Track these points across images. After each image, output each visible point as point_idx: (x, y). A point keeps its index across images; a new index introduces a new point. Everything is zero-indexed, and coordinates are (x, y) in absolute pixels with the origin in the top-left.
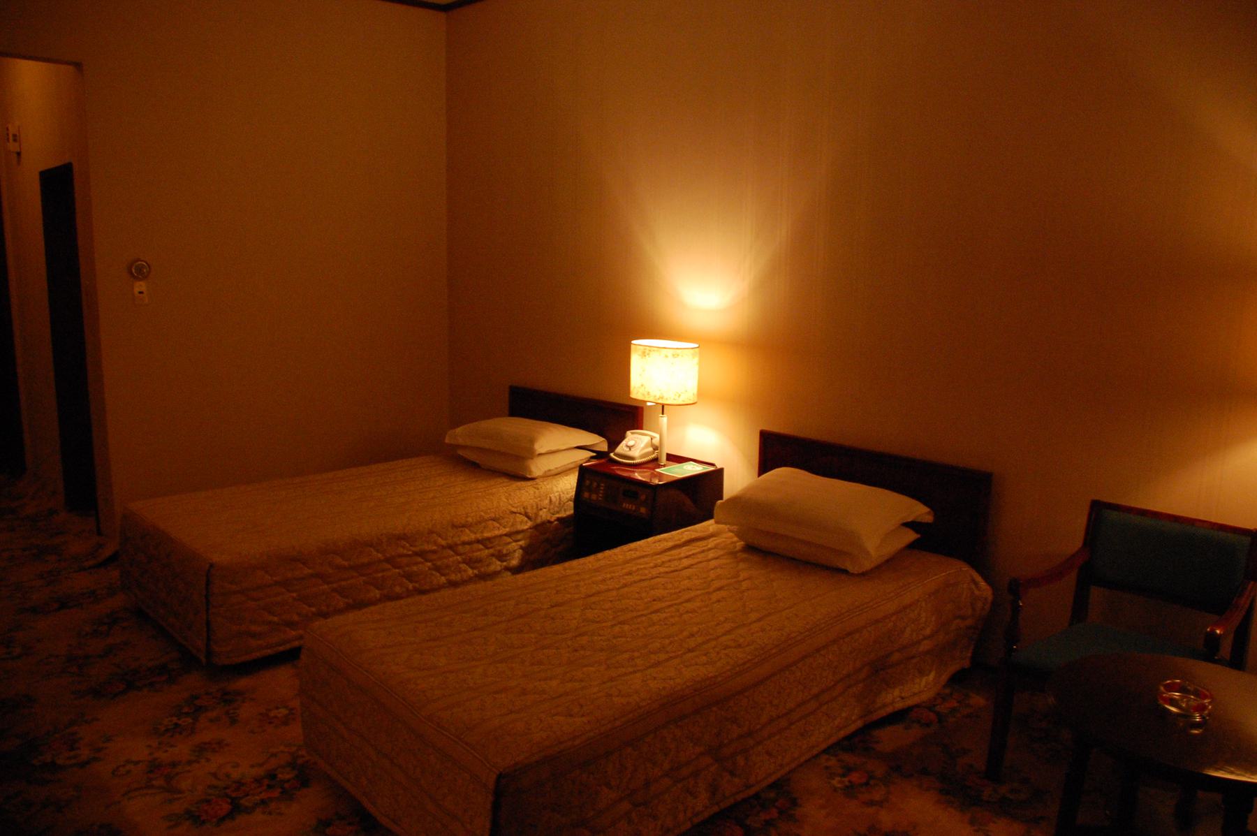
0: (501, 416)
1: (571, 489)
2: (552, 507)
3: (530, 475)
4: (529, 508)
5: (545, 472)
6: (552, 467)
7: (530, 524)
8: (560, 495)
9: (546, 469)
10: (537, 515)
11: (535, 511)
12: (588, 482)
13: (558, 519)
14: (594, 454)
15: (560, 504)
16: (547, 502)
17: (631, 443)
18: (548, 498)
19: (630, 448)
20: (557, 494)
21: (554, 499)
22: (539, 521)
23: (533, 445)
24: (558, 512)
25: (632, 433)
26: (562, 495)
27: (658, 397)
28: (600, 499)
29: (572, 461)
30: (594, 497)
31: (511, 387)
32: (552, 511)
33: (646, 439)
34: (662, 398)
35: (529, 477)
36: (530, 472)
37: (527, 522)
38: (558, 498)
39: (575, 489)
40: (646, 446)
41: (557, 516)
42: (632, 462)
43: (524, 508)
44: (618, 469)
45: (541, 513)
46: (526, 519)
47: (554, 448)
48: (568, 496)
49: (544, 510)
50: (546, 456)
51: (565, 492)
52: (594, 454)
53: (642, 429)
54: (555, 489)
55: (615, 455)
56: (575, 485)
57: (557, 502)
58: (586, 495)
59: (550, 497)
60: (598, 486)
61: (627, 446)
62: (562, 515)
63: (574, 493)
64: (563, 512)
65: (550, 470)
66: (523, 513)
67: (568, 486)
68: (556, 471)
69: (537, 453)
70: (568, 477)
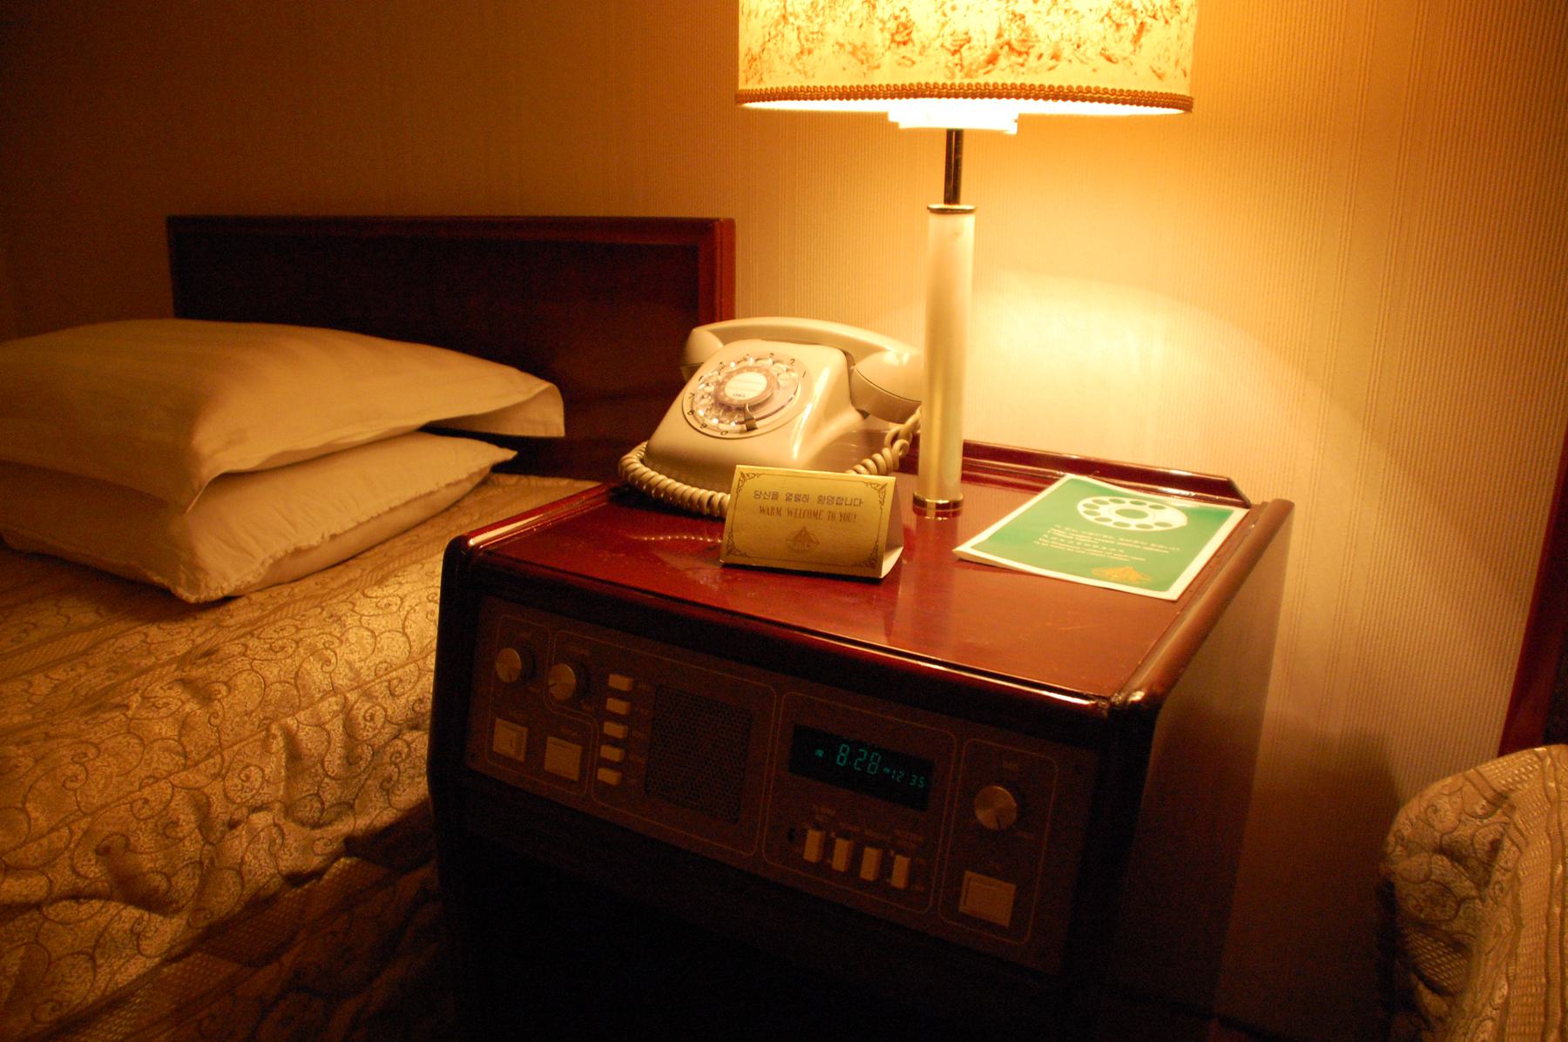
0: (162, 315)
1: (411, 659)
2: (305, 786)
3: (194, 585)
4: (145, 840)
5: (278, 563)
6: (310, 536)
7: (166, 931)
8: (347, 711)
9: (279, 548)
10: (207, 871)
11: (192, 847)
12: (509, 663)
13: (351, 845)
14: (508, 454)
15: (350, 759)
16: (275, 763)
17: (745, 387)
18: (278, 744)
19: (747, 415)
20: (330, 705)
21: (308, 738)
22: (226, 898)
23: (190, 434)
24: (347, 807)
25: (726, 337)
26: (362, 709)
27: (985, 40)
28: (608, 776)
29: (411, 493)
30: (562, 757)
31: (804, 528)
32: (309, 810)
33: (825, 366)
34: (1020, 49)
35: (192, 598)
36: (195, 568)
37: (137, 936)
38: (336, 728)
39: (431, 662)
40: (829, 411)
41: (345, 826)
42: (702, 493)
43: (104, 852)
44: (675, 548)
45: (237, 844)
46: (132, 913)
47: (311, 440)
48: (398, 708)
49: (260, 820)
50: (279, 482)
51: (380, 689)
52: (508, 454)
53: (731, 316)
54: (317, 675)
55: (650, 459)
56: (432, 631)
57: (334, 762)
58: (507, 739)
59: (291, 739)
60: (590, 688)
61: (726, 407)
62: (377, 814)
63: (429, 681)
64: (378, 800)
65: (298, 552)
66: (102, 886)
67: (394, 648)
68: (331, 553)
69: (209, 472)
70: (390, 589)
